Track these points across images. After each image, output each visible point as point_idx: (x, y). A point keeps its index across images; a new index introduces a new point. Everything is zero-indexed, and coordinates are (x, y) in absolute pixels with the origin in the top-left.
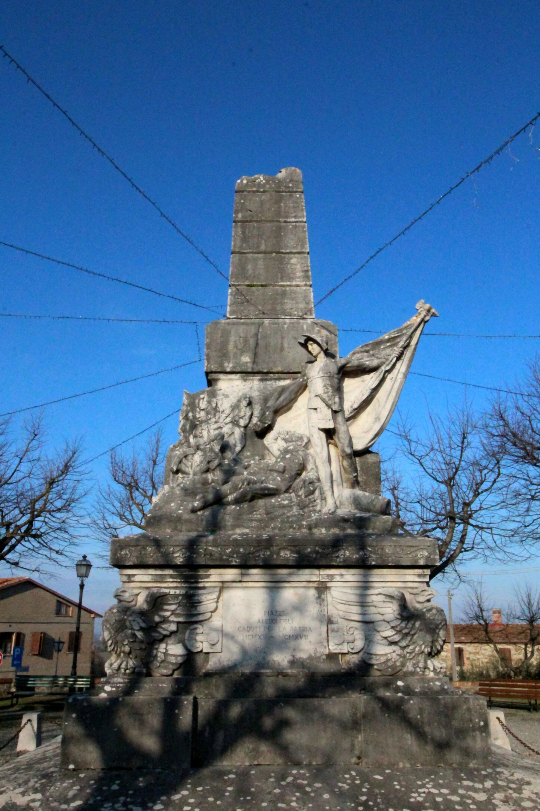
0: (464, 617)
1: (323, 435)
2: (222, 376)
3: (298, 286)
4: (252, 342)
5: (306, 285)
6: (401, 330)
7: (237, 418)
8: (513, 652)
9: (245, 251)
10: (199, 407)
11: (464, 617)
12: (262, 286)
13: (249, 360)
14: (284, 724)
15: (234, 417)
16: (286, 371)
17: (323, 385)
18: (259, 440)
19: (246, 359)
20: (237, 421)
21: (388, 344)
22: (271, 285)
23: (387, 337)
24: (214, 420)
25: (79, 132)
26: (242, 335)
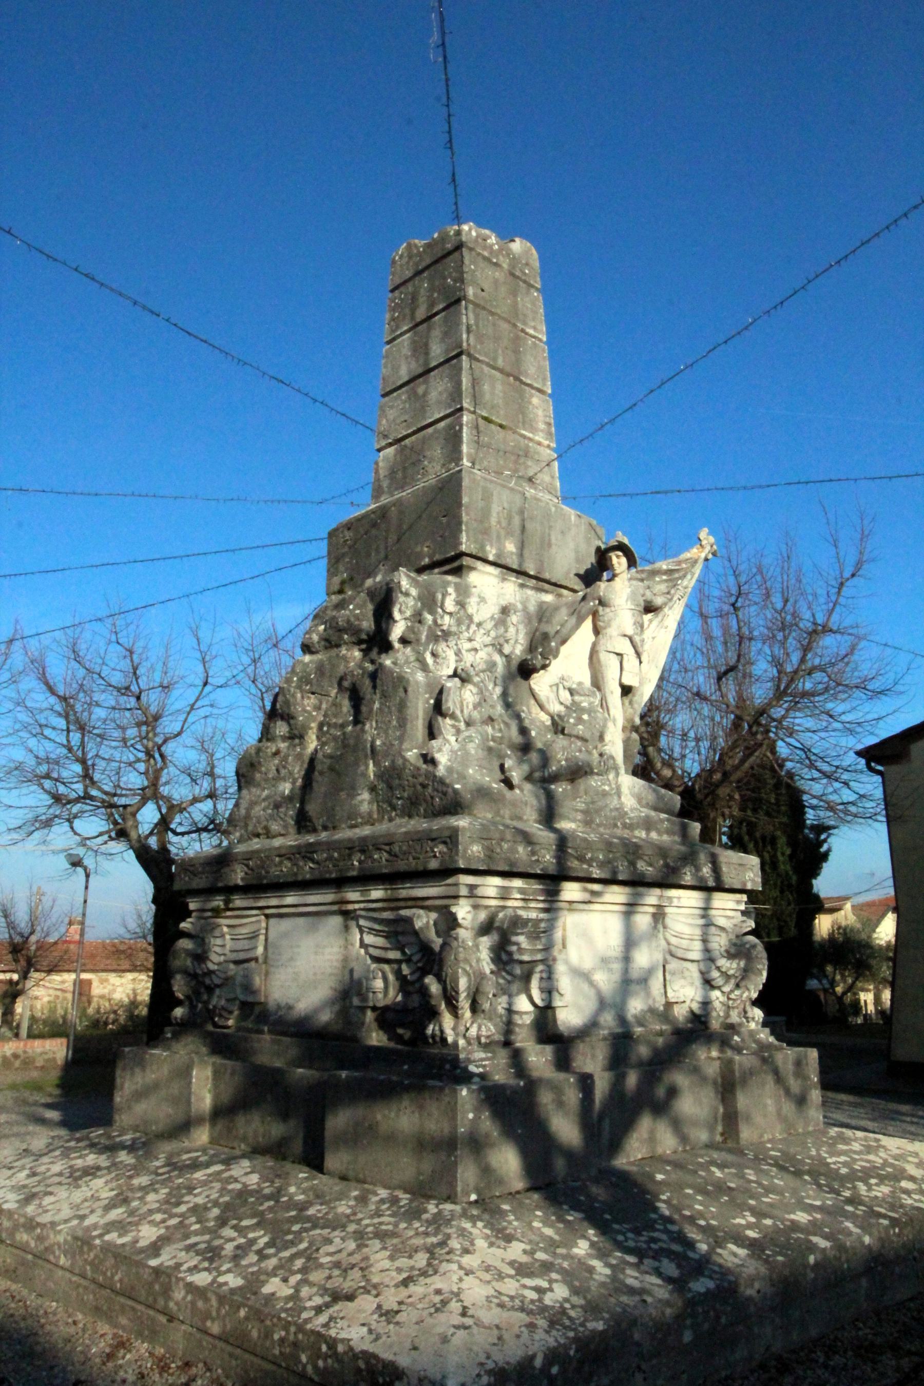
0: (122, 931)
1: (619, 690)
2: (479, 565)
3: (539, 444)
4: (517, 521)
5: (548, 446)
6: (679, 563)
7: (502, 641)
8: (95, 984)
9: (481, 358)
10: (442, 607)
11: (122, 931)
12: (501, 426)
13: (514, 550)
14: (673, 1092)
15: (496, 637)
16: (553, 580)
17: (632, 621)
18: (523, 681)
19: (510, 547)
20: (501, 645)
21: (664, 577)
22: (511, 429)
23: (665, 567)
24: (466, 635)
25: (810, 278)
26: (506, 505)
